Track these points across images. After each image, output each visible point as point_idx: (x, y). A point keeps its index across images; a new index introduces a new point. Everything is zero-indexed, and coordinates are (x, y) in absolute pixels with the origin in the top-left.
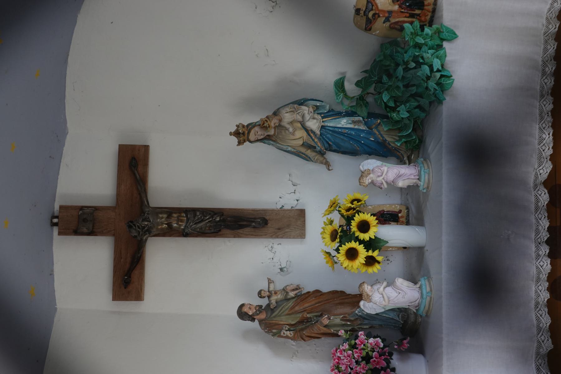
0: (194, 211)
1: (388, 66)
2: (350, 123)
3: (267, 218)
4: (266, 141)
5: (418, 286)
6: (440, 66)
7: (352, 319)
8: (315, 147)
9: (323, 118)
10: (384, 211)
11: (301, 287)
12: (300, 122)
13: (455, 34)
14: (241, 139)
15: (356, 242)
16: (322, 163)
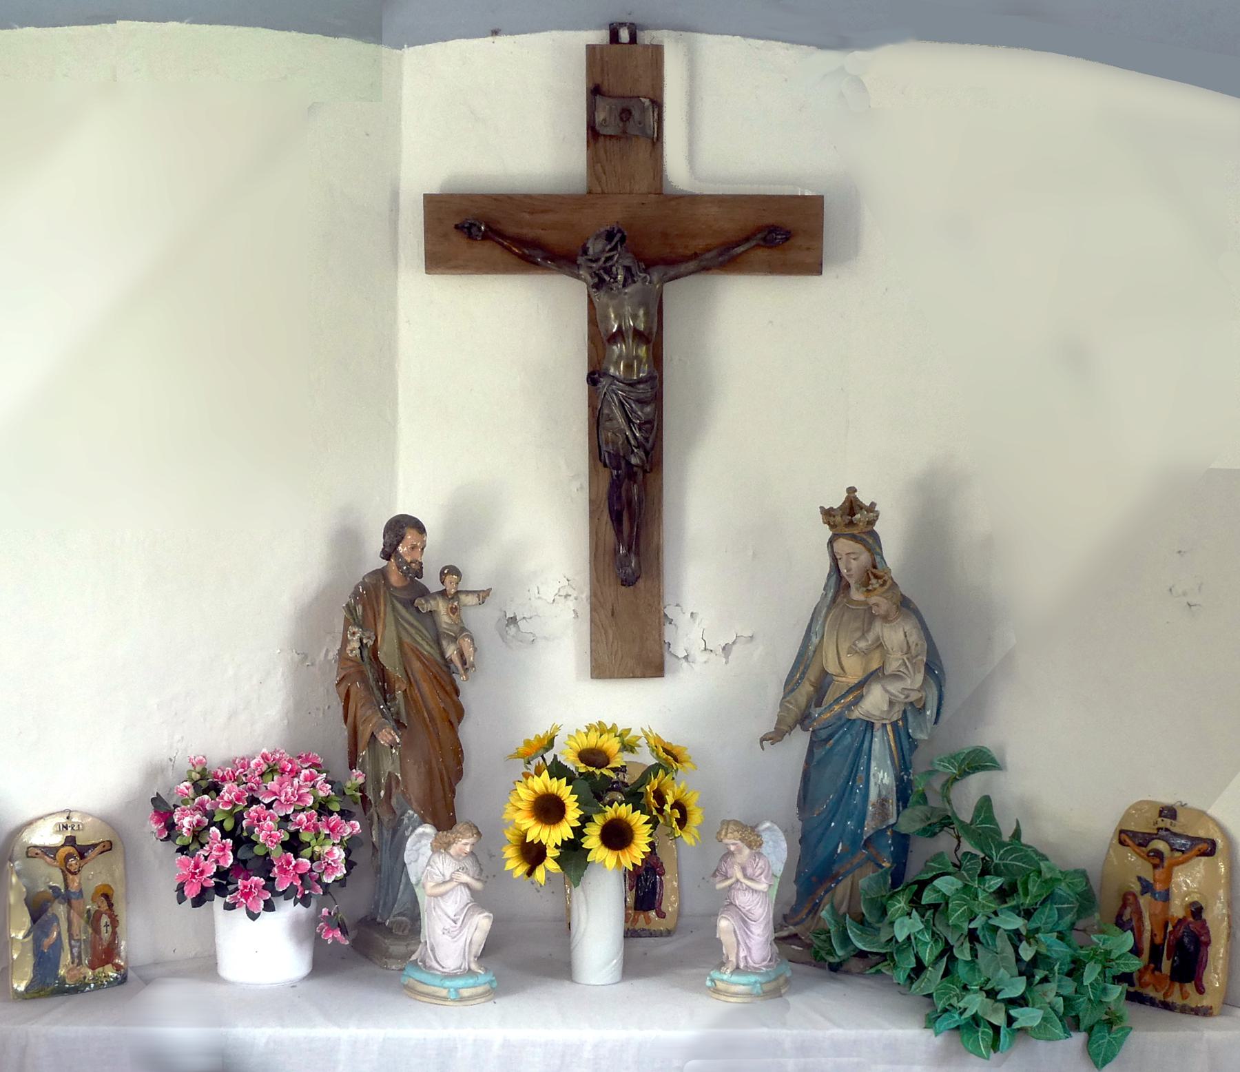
0: (656, 399)
1: (1026, 893)
2: (879, 795)
3: (641, 584)
4: (834, 579)
5: (474, 967)
6: (1024, 1025)
7: (394, 802)
8: (819, 704)
9: (894, 725)
10: (660, 875)
11: (471, 671)
12: (881, 668)
13: (1105, 1062)
14: (838, 519)
15: (578, 819)
16: (779, 722)
